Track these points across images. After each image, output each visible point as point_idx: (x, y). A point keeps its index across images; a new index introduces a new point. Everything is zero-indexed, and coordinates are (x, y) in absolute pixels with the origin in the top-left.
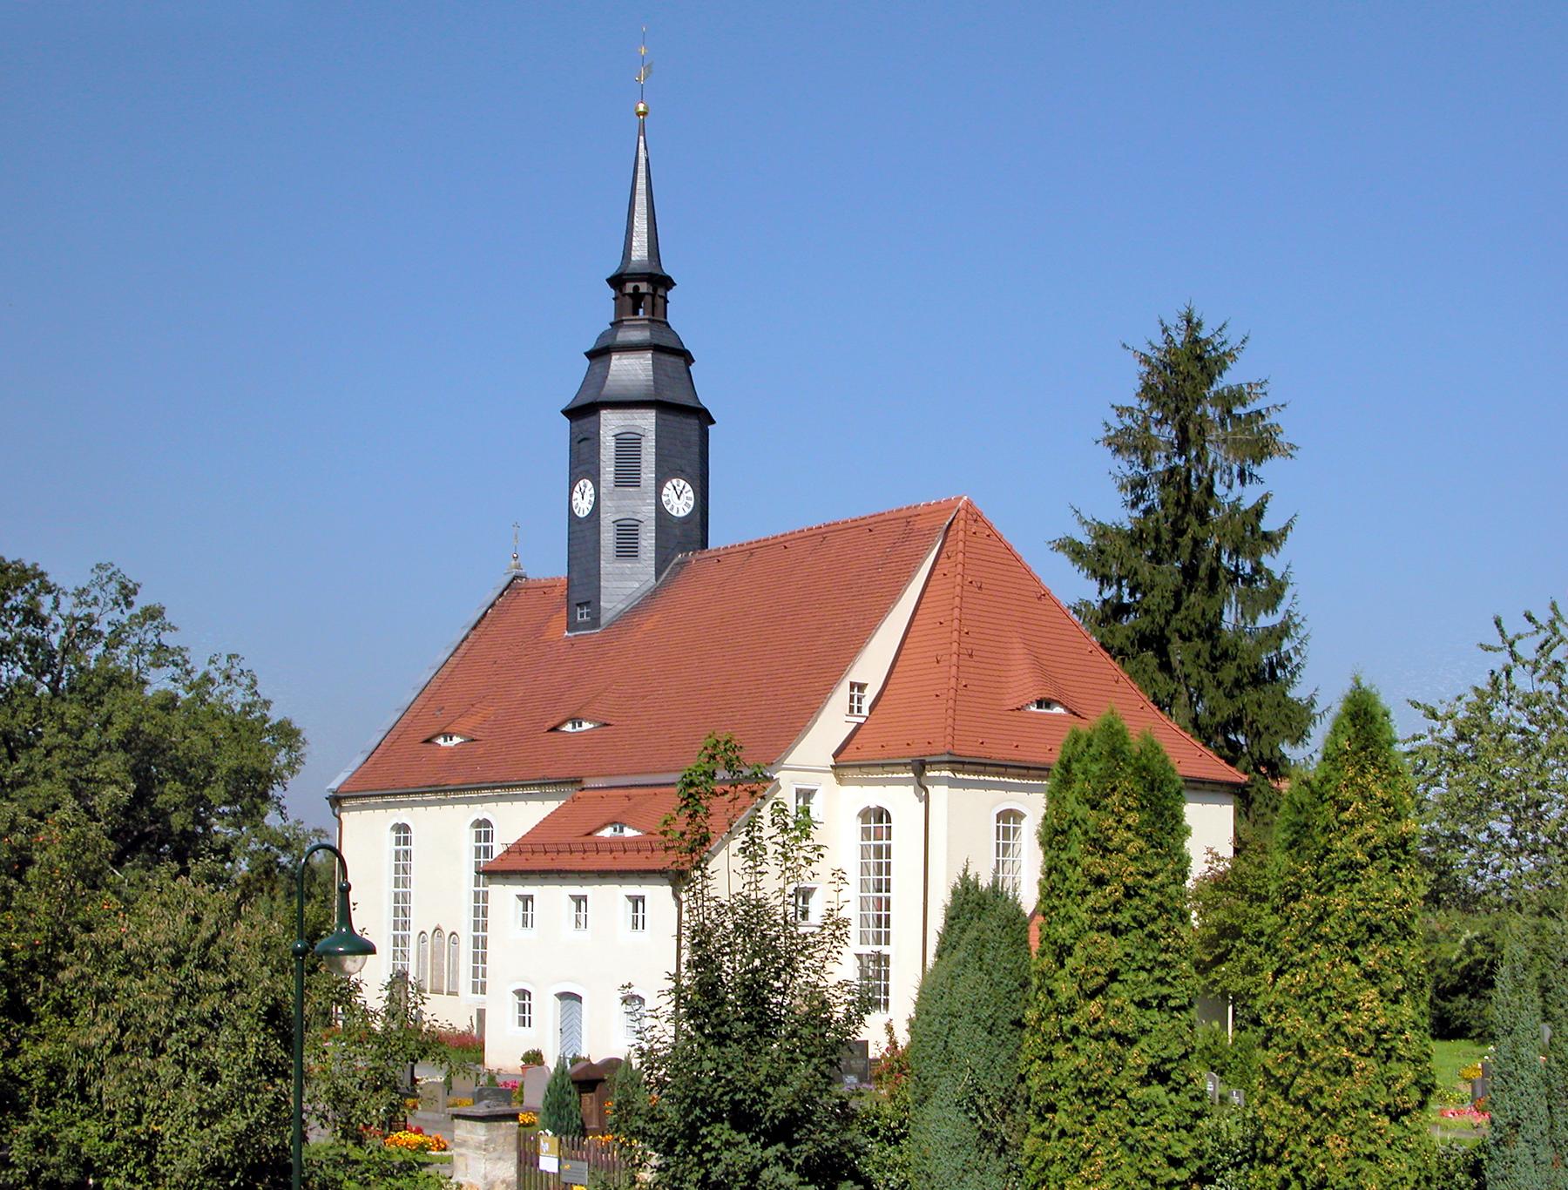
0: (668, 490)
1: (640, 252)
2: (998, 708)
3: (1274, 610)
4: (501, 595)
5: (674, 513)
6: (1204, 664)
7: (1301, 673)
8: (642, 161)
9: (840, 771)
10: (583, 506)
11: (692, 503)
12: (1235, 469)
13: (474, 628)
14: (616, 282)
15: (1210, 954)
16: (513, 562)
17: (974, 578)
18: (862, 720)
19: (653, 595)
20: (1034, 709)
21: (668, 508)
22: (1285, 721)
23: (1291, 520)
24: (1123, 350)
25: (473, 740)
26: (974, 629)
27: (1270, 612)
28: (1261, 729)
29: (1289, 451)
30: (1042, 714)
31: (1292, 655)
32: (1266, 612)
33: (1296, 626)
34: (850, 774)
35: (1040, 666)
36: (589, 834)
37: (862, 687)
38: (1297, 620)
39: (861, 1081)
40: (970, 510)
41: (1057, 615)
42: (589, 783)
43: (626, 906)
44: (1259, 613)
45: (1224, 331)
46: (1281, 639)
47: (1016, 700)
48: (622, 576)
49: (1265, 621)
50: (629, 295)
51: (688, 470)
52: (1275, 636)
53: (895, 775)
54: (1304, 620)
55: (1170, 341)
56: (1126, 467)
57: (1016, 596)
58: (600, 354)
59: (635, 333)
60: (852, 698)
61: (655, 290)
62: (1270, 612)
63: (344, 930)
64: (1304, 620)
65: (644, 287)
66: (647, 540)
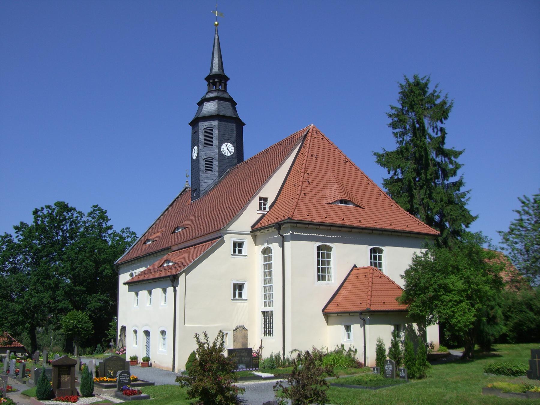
0: (224, 147)
1: (216, 69)
2: (321, 203)
8: (216, 41)
10: (195, 156)
14: (208, 79)
18: (266, 213)
19: (218, 183)
21: (224, 153)
26: (311, 172)
34: (258, 233)
35: (342, 186)
36: (161, 266)
37: (266, 199)
40: (314, 129)
41: (353, 169)
47: (330, 200)
48: (207, 178)
49: (452, 180)
55: (407, 81)
57: (334, 161)
58: (201, 104)
60: (260, 204)
61: (221, 80)
66: (215, 164)
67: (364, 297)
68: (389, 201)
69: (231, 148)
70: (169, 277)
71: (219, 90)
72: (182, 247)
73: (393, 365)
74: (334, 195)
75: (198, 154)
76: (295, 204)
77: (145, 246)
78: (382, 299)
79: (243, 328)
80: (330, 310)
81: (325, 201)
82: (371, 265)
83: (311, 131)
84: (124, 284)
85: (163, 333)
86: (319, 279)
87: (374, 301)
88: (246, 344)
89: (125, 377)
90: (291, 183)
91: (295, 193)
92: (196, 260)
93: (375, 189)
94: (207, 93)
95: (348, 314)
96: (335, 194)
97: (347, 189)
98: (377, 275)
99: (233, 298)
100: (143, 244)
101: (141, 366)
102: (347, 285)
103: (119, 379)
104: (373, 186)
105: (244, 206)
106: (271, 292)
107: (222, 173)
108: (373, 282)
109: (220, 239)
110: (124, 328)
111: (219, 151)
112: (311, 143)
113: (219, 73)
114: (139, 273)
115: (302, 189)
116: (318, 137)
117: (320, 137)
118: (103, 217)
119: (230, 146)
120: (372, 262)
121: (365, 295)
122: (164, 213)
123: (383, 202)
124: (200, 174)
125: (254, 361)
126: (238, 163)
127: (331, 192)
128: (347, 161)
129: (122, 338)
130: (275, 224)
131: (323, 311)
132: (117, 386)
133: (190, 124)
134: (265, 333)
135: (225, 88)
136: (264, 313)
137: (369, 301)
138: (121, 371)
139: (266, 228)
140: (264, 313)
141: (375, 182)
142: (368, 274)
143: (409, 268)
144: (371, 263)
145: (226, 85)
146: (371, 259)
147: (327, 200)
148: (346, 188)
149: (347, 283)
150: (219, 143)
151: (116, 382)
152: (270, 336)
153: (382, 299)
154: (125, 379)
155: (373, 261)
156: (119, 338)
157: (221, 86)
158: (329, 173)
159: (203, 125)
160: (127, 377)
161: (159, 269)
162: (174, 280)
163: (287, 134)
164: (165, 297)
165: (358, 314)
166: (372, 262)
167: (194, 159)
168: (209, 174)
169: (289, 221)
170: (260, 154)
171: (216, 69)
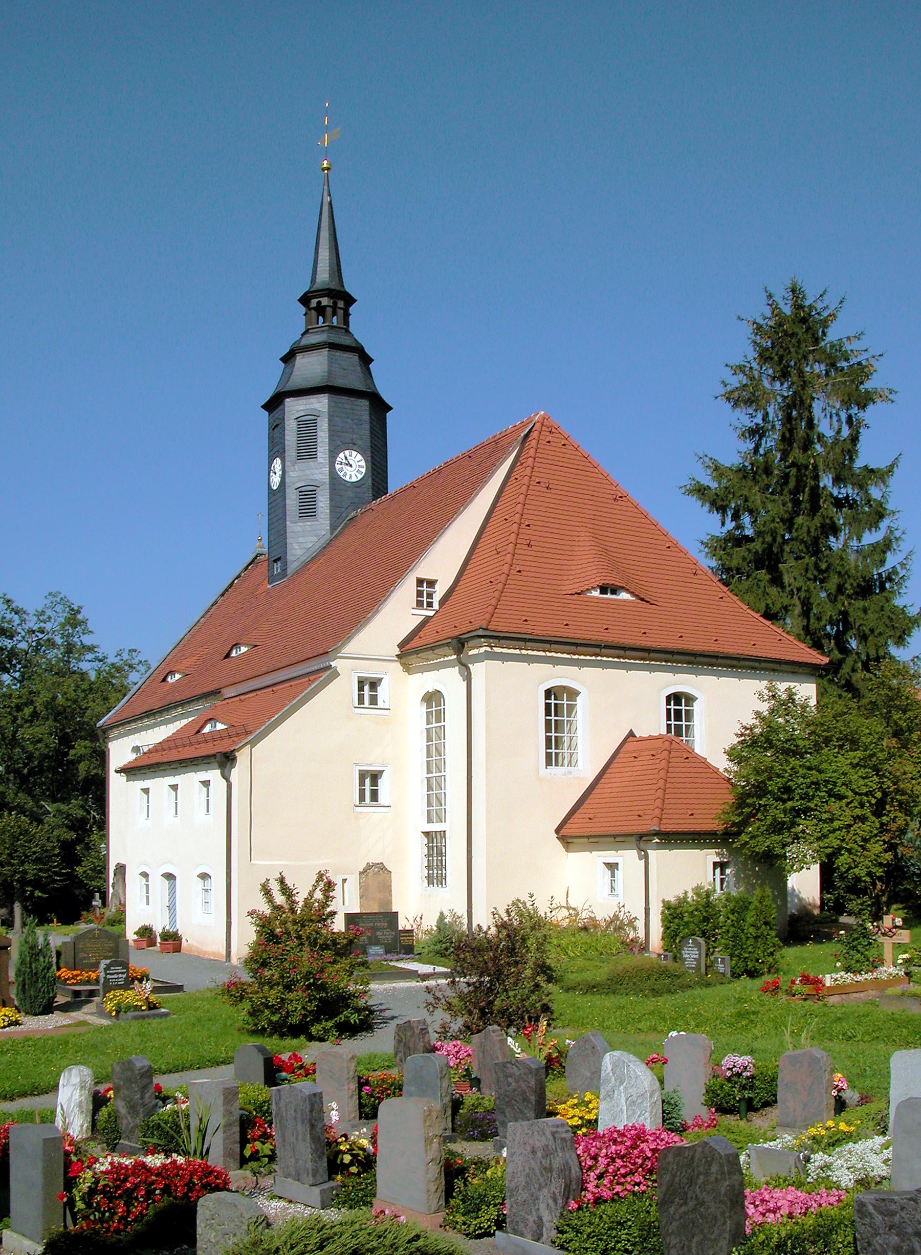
3: (877, 528)
4: (246, 569)
5: (347, 479)
6: (812, 577)
7: (906, 584)
9: (403, 660)
10: (276, 480)
11: (363, 470)
12: (843, 416)
13: (223, 595)
14: (305, 300)
15: (739, 815)
16: (258, 544)
17: (540, 480)
18: (431, 613)
19: (329, 544)
20: (596, 593)
21: (341, 474)
22: (888, 622)
23: (896, 459)
24: (740, 322)
25: (256, 646)
27: (873, 529)
28: (868, 632)
29: (888, 396)
30: (604, 599)
31: (899, 569)
32: (870, 530)
33: (897, 539)
34: (412, 659)
36: (198, 732)
37: (431, 583)
38: (897, 534)
39: (387, 952)
40: (546, 423)
42: (228, 692)
43: (200, 792)
44: (864, 529)
45: (825, 297)
46: (884, 552)
47: (576, 585)
49: (870, 538)
50: (313, 308)
51: (360, 442)
52: (878, 550)
53: (446, 659)
54: (903, 533)
55: (774, 307)
56: (744, 418)
59: (315, 337)
60: (420, 594)
62: (873, 529)
63: (757, 869)
64: (903, 533)
65: (325, 301)
66: (323, 502)
67: (648, 802)
68: (714, 589)
69: (358, 464)
70: (214, 756)
71: (332, 327)
72: (247, 690)
73: (699, 950)
74: (587, 574)
75: (283, 477)
76: (497, 594)
77: (165, 687)
78: (688, 806)
79: (381, 867)
80: (571, 831)
81: (566, 587)
82: (669, 731)
83: (538, 426)
84: (117, 772)
85: (204, 876)
86: (549, 762)
87: (670, 811)
88: (389, 902)
89: (118, 973)
90: (489, 546)
91: (498, 569)
92: (273, 719)
93: (684, 560)
94: (303, 334)
95: (612, 839)
96: (589, 573)
97: (619, 560)
98: (679, 754)
99: (357, 803)
100: (162, 682)
101: (159, 949)
102: (613, 775)
103: (105, 978)
104: (678, 555)
105: (383, 598)
106: (443, 791)
107: (338, 521)
108: (670, 770)
109: (330, 672)
110: (121, 869)
111: (330, 472)
112: (538, 455)
113: (333, 287)
114: (151, 747)
115: (515, 561)
116: (556, 440)
117: (558, 440)
118: (74, 620)
119: (357, 459)
120: (671, 725)
121: (650, 797)
122: (208, 611)
123: (700, 591)
124: (288, 522)
125: (405, 940)
126: (375, 498)
127: (580, 567)
128: (621, 497)
129: (117, 891)
130: (449, 640)
131: (557, 831)
132: (101, 992)
133: (265, 407)
134: (430, 880)
135: (346, 322)
136: (427, 834)
137: (657, 811)
138: (108, 961)
139: (432, 648)
140: (427, 834)
141: (683, 544)
142: (660, 752)
143: (736, 740)
144: (669, 726)
145: (347, 315)
146: (669, 719)
147: (572, 587)
148: (615, 559)
149: (615, 770)
150: (330, 451)
151: (97, 981)
152: (431, 886)
153: (688, 806)
154: (118, 978)
155: (673, 722)
156: (111, 890)
157: (335, 317)
158: (577, 524)
159: (294, 408)
160: (123, 973)
161: (193, 739)
162: (226, 760)
163: (485, 436)
164: (208, 800)
165: (633, 839)
166: (671, 725)
167: (275, 488)
168: (309, 523)
169: (480, 632)
170: (424, 479)
171: (324, 276)
